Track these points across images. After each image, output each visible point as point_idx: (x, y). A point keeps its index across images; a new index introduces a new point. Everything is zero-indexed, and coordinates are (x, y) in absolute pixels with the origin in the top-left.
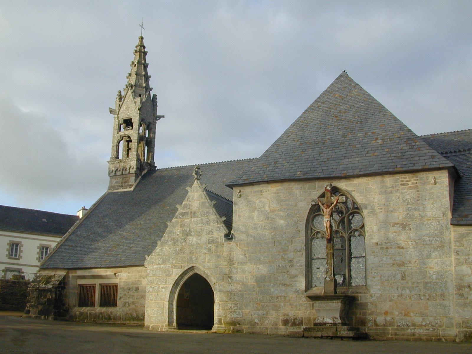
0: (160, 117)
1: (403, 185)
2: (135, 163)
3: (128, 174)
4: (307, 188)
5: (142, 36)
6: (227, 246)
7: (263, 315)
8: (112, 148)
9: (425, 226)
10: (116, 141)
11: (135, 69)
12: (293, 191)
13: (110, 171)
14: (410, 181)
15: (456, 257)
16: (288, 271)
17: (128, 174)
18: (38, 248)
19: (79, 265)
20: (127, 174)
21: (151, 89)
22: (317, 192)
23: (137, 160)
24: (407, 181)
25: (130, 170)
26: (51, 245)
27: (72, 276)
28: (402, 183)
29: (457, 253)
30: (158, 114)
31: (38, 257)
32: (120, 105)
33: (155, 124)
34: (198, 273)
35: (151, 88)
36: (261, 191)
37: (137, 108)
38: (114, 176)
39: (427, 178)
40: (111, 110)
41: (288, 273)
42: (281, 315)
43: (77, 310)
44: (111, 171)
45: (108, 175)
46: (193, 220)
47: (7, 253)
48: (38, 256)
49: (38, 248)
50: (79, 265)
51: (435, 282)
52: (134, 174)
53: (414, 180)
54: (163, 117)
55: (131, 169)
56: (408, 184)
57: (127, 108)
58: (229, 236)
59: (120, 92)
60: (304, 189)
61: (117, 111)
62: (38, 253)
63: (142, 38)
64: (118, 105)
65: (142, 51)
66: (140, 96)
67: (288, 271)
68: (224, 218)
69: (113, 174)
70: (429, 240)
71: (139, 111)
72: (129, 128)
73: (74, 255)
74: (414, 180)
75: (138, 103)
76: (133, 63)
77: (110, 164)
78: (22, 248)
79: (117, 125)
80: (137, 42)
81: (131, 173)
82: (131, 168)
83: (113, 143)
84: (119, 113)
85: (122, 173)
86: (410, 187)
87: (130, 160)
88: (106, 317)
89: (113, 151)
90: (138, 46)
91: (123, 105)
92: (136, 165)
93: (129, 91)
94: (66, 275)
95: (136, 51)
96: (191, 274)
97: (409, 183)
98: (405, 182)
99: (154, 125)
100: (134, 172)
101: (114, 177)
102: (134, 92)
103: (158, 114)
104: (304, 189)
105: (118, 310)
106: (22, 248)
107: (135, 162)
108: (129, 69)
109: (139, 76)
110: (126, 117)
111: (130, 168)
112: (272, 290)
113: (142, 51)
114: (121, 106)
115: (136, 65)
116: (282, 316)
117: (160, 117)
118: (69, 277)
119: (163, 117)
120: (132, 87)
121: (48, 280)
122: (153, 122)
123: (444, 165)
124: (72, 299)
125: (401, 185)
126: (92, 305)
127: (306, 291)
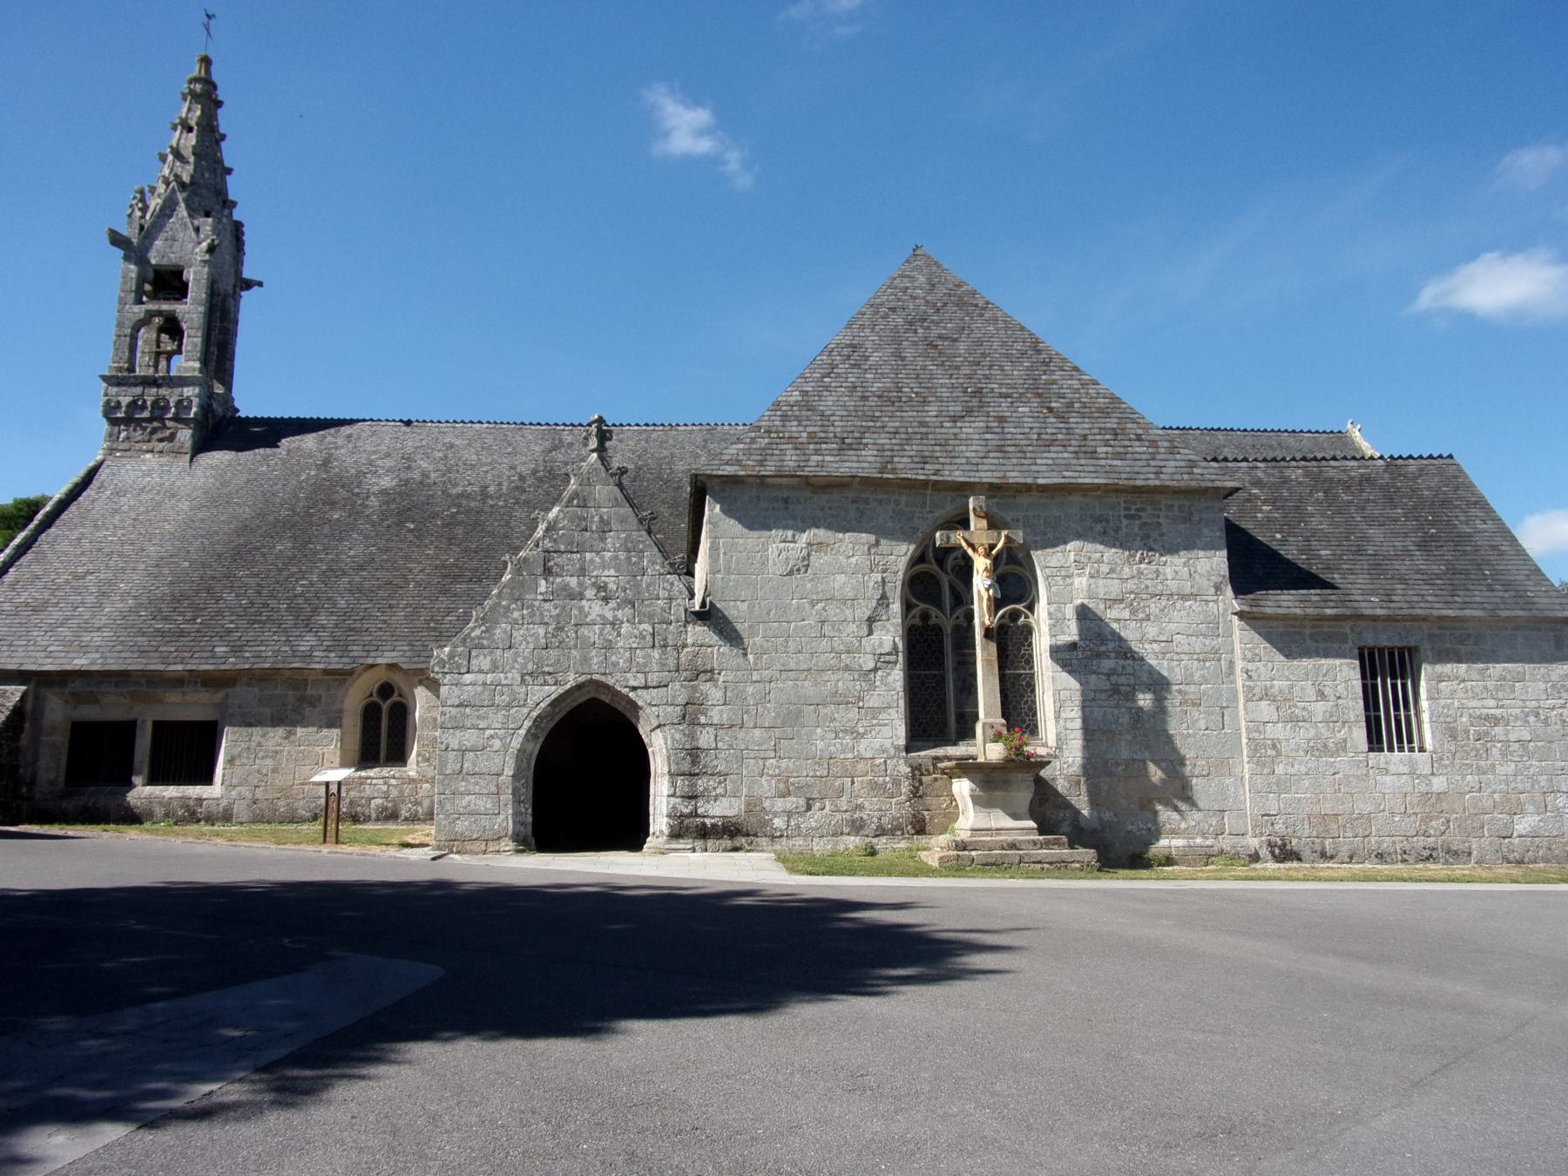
4: (903, 503)
8: (115, 342)
10: (129, 324)
13: (108, 403)
15: (1247, 683)
19: (76, 661)
24: (1138, 510)
29: (1247, 673)
30: (247, 273)
33: (237, 299)
35: (232, 202)
45: (101, 415)
46: (588, 559)
50: (76, 661)
54: (260, 284)
56: (1140, 517)
64: (138, 227)
65: (207, 95)
73: (47, 632)
83: (120, 325)
97: (1142, 514)
113: (207, 95)
117: (248, 285)
119: (260, 284)
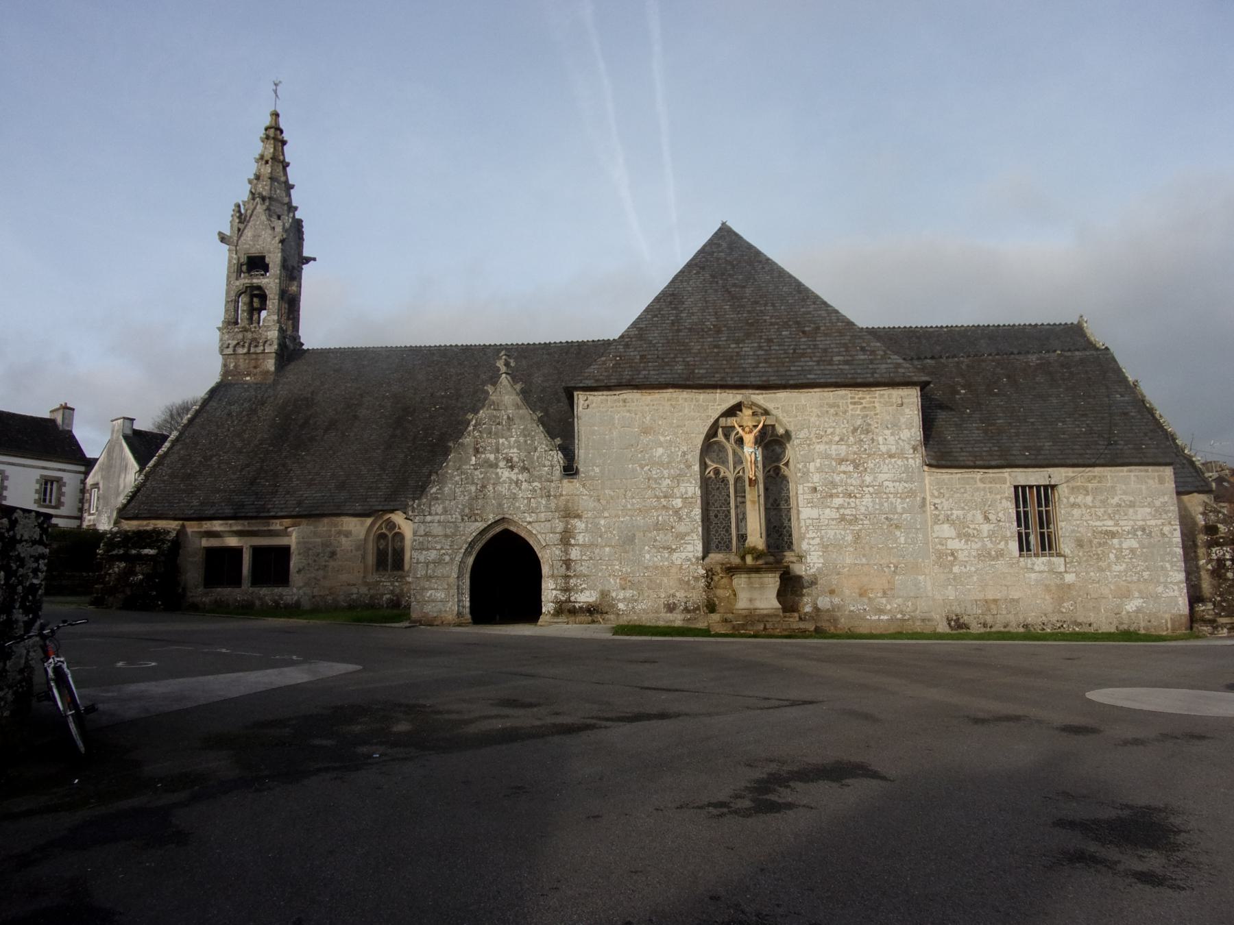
0: (308, 260)
1: (854, 403)
2: (277, 335)
3: (262, 353)
5: (275, 111)
6: (568, 486)
7: (633, 596)
9: (888, 465)
10: (233, 294)
11: (268, 169)
12: (678, 403)
14: (864, 398)
16: (672, 527)
17: (262, 353)
18: (37, 483)
20: (260, 353)
21: (296, 208)
22: (719, 407)
23: (279, 330)
24: (860, 398)
25: (266, 347)
26: (62, 478)
27: (193, 532)
28: (853, 400)
30: (306, 253)
31: (37, 498)
32: (239, 230)
34: (513, 529)
36: (624, 401)
37: (277, 239)
38: (231, 354)
39: (890, 396)
40: (222, 235)
41: (673, 530)
42: (663, 596)
43: (197, 592)
44: (225, 346)
47: (37, 486)
48: (37, 496)
49: (37, 483)
51: (903, 547)
52: (274, 355)
53: (870, 398)
54: (314, 259)
55: (266, 345)
56: (861, 403)
57: (256, 237)
58: (570, 470)
59: (239, 206)
60: (697, 401)
61: (235, 238)
62: (37, 491)
63: (276, 115)
64: (237, 229)
65: (275, 135)
66: (279, 218)
67: (672, 527)
68: (558, 441)
69: (230, 351)
70: (894, 487)
71: (280, 245)
72: (257, 271)
74: (870, 398)
75: (279, 229)
76: (262, 157)
77: (223, 333)
78: (5, 481)
79: (235, 264)
80: (267, 121)
81: (266, 351)
82: (268, 343)
84: (237, 243)
85: (249, 350)
86: (865, 407)
87: (265, 329)
88: (270, 604)
89: (227, 311)
90: (271, 128)
91: (246, 231)
92: (278, 338)
93: (259, 206)
94: (179, 530)
95: (268, 137)
96: (498, 529)
98: (856, 400)
99: (299, 271)
100: (274, 351)
101: (232, 356)
102: (268, 209)
103: (306, 253)
104: (697, 401)
105: (295, 591)
106: (5, 481)
107: (276, 333)
108: (251, 169)
109: (275, 181)
110: (254, 251)
111: (265, 342)
112: (647, 556)
113: (275, 135)
114: (243, 230)
115: (270, 162)
116: (664, 597)
117: (308, 260)
118: (185, 534)
119: (314, 259)
120: (263, 199)
121: (141, 538)
122: (299, 266)
123: (915, 379)
124: (193, 574)
125: (851, 403)
126: (236, 581)
127: (703, 558)
